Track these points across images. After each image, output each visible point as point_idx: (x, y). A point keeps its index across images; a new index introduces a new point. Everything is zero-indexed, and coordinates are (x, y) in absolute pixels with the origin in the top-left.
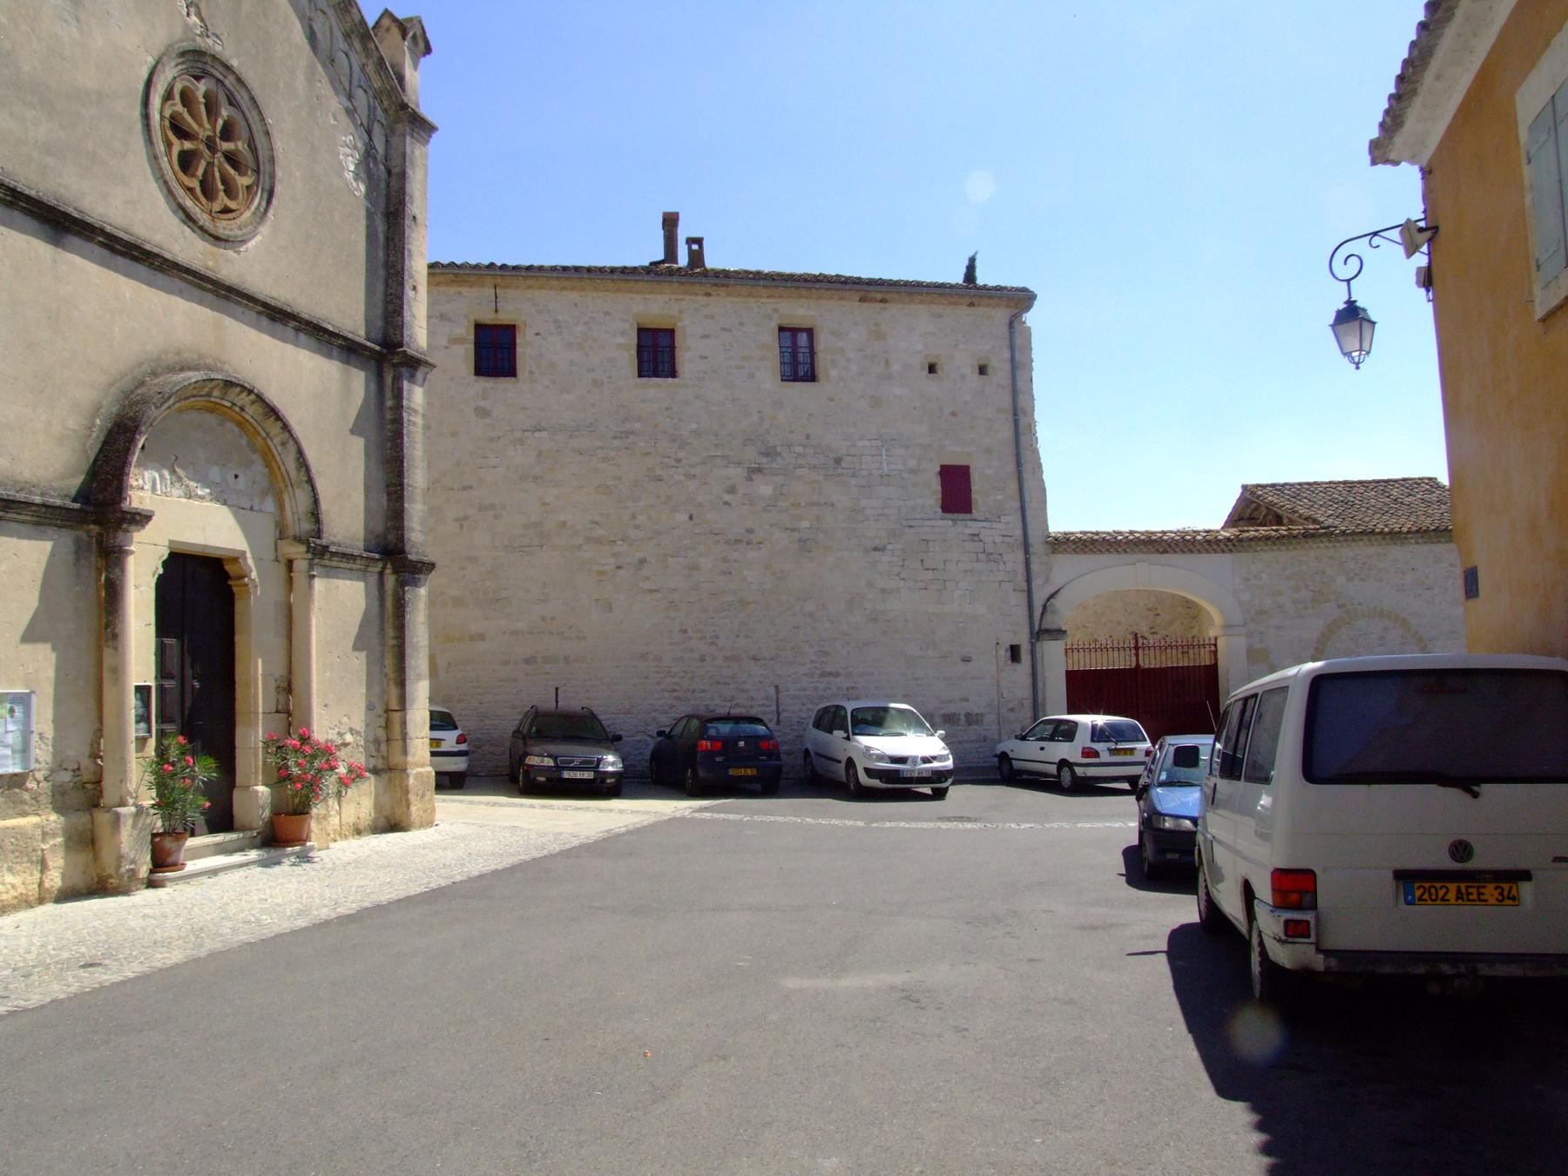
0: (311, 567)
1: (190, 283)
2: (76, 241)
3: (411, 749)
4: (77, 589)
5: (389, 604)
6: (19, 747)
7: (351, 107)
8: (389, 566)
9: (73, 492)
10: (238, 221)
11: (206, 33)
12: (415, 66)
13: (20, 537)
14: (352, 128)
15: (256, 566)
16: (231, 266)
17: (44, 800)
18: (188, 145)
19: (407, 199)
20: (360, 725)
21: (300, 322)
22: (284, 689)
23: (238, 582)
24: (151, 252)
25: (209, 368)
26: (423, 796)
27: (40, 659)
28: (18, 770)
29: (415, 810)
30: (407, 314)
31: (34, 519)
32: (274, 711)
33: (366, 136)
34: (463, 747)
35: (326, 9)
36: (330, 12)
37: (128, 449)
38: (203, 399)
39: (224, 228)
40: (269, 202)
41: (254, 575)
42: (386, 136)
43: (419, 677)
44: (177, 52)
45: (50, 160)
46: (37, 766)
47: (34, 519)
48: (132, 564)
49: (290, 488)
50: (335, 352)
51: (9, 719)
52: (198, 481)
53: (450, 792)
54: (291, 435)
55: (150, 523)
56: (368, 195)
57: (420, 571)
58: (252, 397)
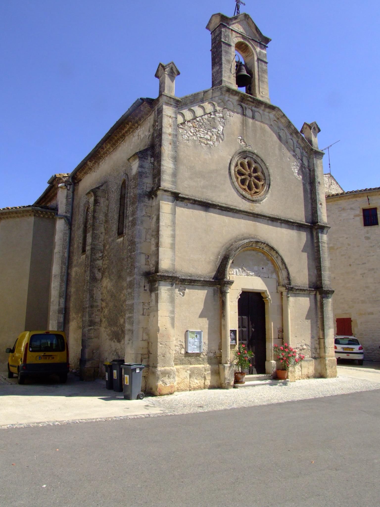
0: (288, 294)
1: (245, 215)
2: (212, 209)
3: (327, 350)
4: (214, 303)
5: (319, 304)
6: (198, 346)
7: (295, 154)
8: (318, 292)
9: (213, 276)
10: (260, 195)
11: (246, 145)
12: (316, 136)
13: (198, 289)
14: (296, 160)
15: (270, 294)
16: (258, 208)
17: (206, 360)
18: (243, 177)
19: (316, 177)
20: (309, 343)
21: (281, 221)
22: (281, 331)
23: (266, 299)
24: (233, 209)
25: (252, 238)
26: (332, 367)
27: (204, 322)
28: (198, 352)
29: (329, 371)
30: (319, 213)
31: (202, 285)
32: (278, 338)
33: (301, 162)
34: (361, 351)
35: (284, 129)
36: (285, 129)
37: (226, 264)
38: (250, 247)
39: (255, 198)
40: (269, 187)
41: (270, 297)
42: (308, 160)
43: (330, 328)
44: (238, 153)
45: (204, 190)
46: (204, 351)
47: (202, 285)
48: (228, 296)
49: (280, 270)
50: (295, 228)
51: (196, 338)
52: (250, 271)
53: (358, 366)
54: (279, 255)
55: (233, 284)
56: (303, 179)
57: (329, 293)
58: (265, 245)
